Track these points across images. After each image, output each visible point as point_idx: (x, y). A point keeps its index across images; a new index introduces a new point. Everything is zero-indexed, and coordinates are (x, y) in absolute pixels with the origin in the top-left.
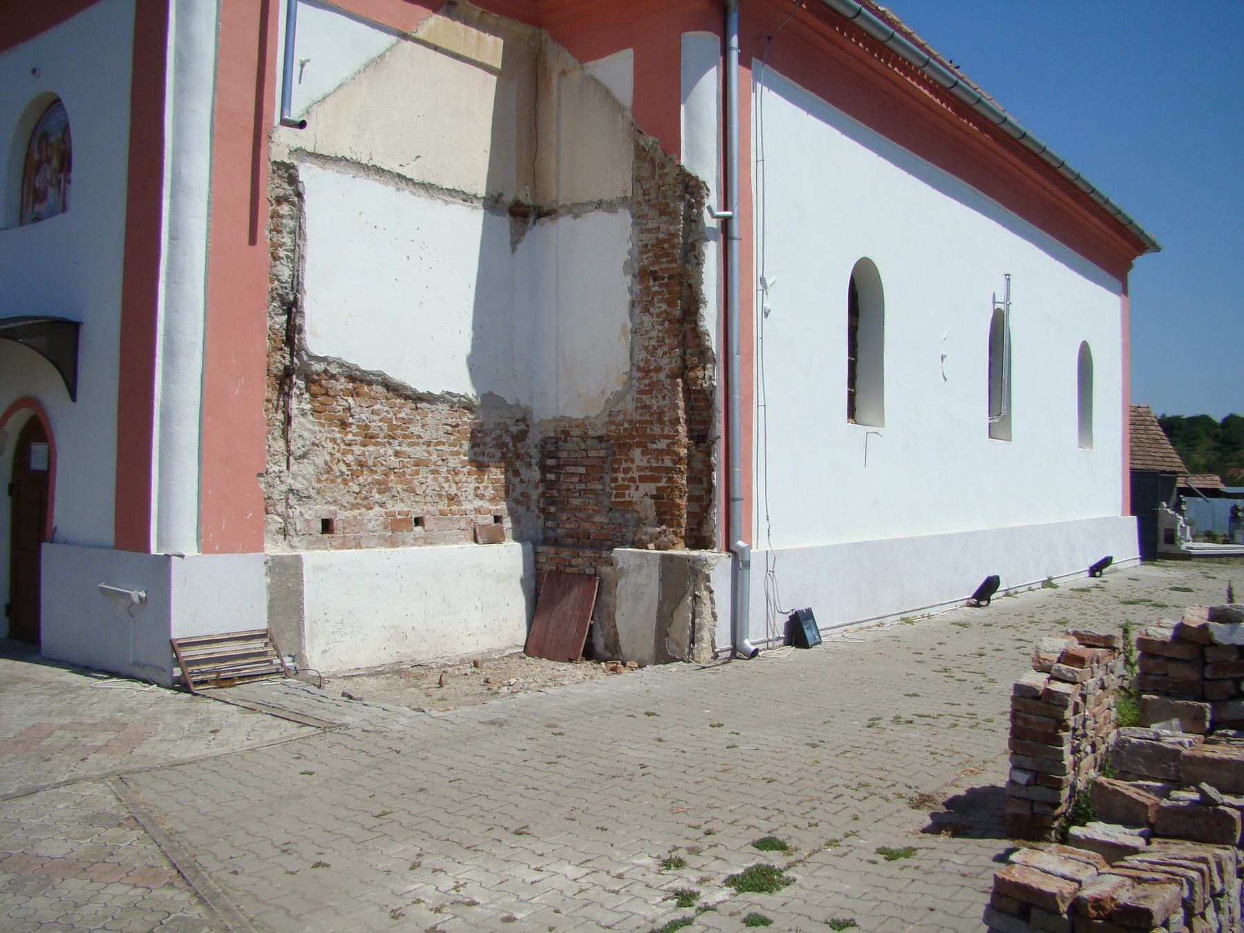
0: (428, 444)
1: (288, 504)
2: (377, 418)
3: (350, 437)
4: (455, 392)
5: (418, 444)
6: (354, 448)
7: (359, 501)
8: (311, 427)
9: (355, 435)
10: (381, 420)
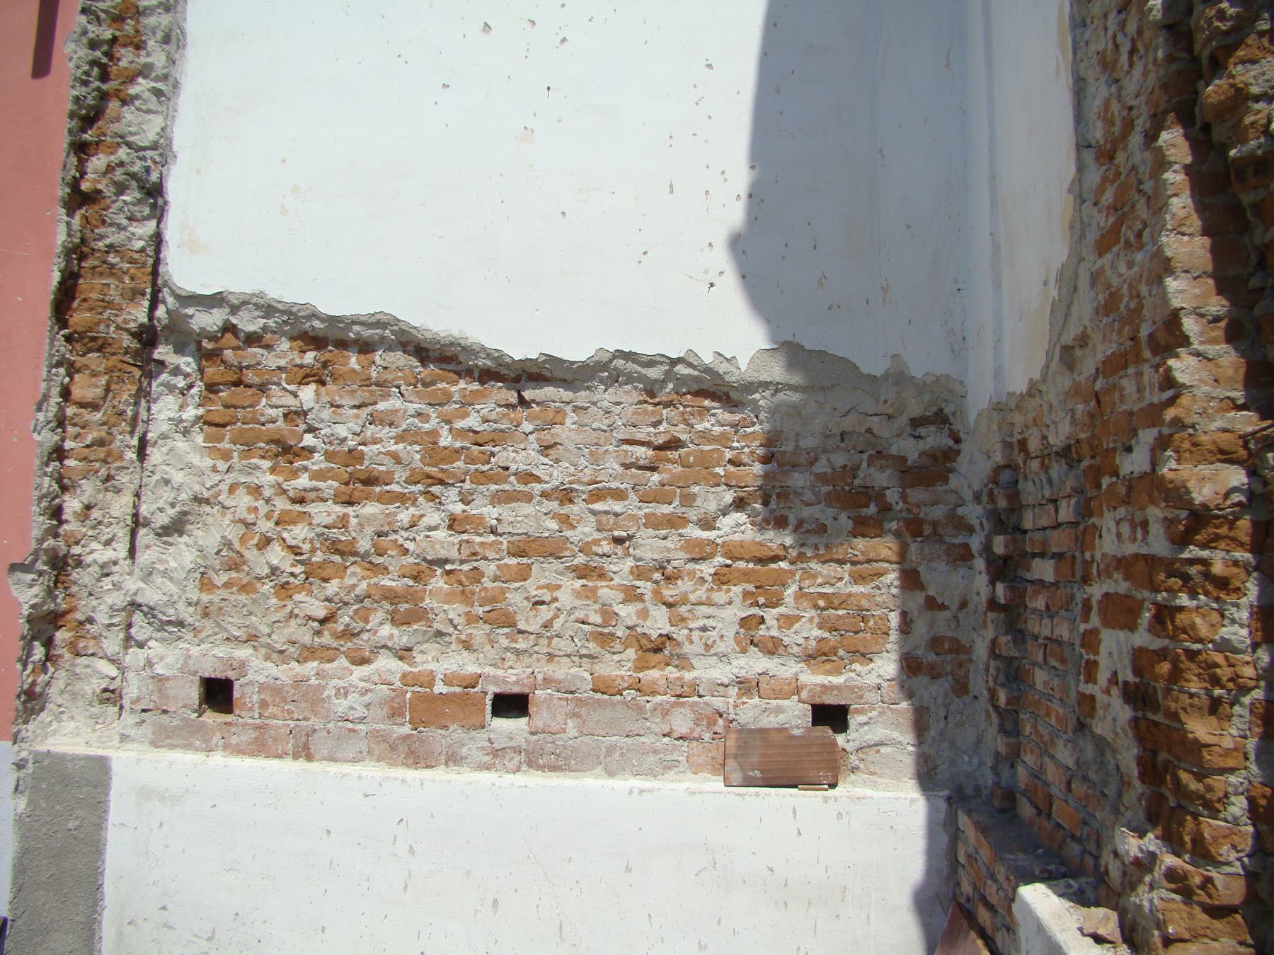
0: (566, 496)
1: (128, 638)
2: (384, 432)
3: (303, 481)
4: (647, 348)
5: (528, 498)
6: (312, 508)
7: (327, 639)
8: (196, 459)
9: (319, 475)
10: (400, 438)
